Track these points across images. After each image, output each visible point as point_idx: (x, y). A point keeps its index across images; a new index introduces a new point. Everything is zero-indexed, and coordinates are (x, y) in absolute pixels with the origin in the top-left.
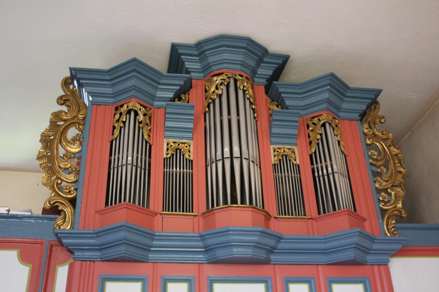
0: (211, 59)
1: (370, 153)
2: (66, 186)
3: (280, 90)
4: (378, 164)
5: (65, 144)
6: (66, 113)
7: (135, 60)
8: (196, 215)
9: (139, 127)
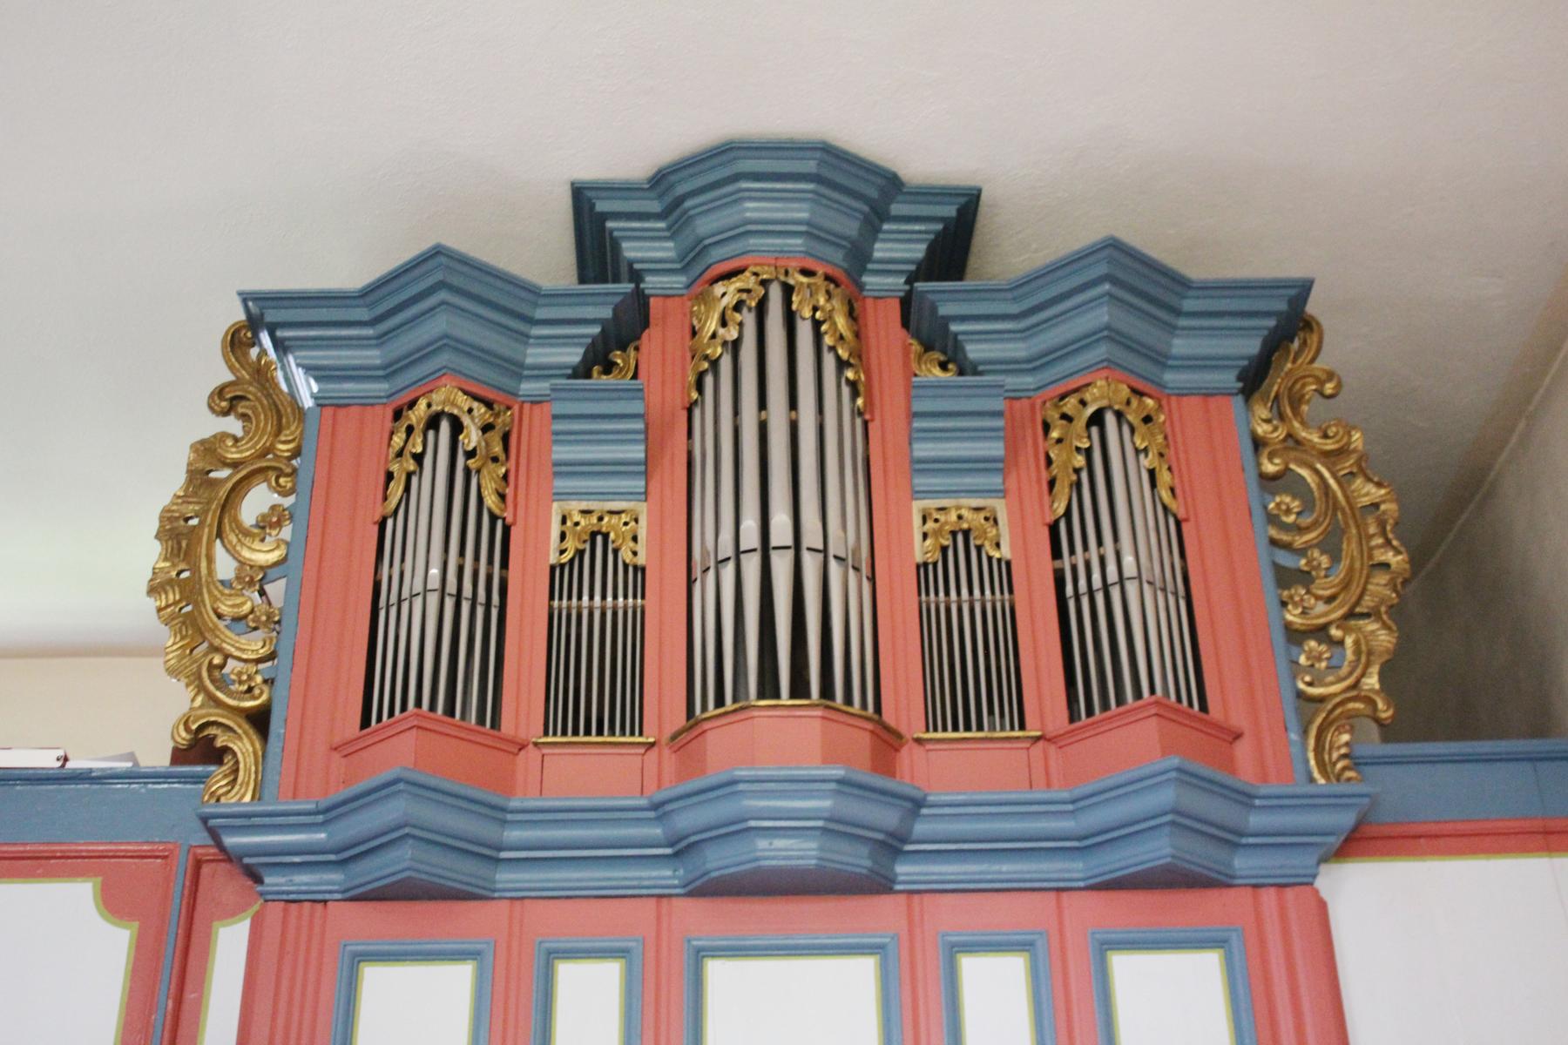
0: (705, 226)
1: (1272, 505)
2: (240, 674)
3: (944, 310)
4: (1299, 541)
5: (235, 540)
6: (236, 440)
7: (438, 253)
8: (652, 745)
9: (467, 472)
